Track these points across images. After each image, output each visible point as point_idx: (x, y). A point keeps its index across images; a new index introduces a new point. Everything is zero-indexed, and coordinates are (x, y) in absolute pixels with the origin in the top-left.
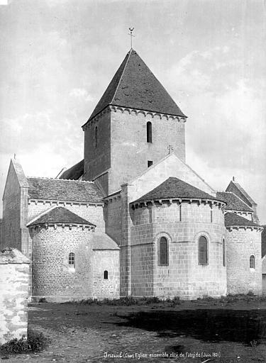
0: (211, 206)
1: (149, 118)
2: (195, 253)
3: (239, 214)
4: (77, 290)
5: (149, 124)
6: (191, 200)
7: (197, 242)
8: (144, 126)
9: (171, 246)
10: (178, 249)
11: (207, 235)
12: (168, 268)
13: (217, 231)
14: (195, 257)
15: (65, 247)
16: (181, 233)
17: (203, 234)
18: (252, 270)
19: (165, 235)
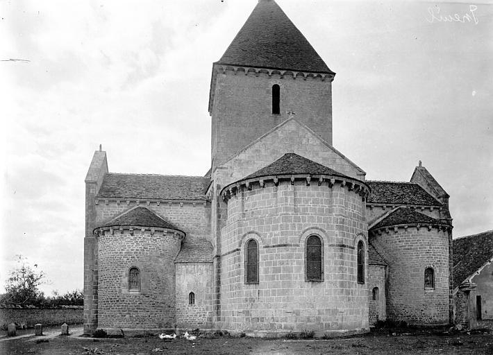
0: (331, 186)
1: (278, 82)
2: (298, 263)
3: (419, 211)
4: (142, 320)
5: (276, 89)
6: (293, 178)
7: (303, 245)
8: (268, 92)
9: (263, 255)
10: (271, 258)
11: (322, 235)
12: (259, 288)
13: (340, 228)
14: (298, 270)
15: (125, 259)
16: (276, 232)
17: (314, 232)
18: (430, 290)
19: (253, 236)
